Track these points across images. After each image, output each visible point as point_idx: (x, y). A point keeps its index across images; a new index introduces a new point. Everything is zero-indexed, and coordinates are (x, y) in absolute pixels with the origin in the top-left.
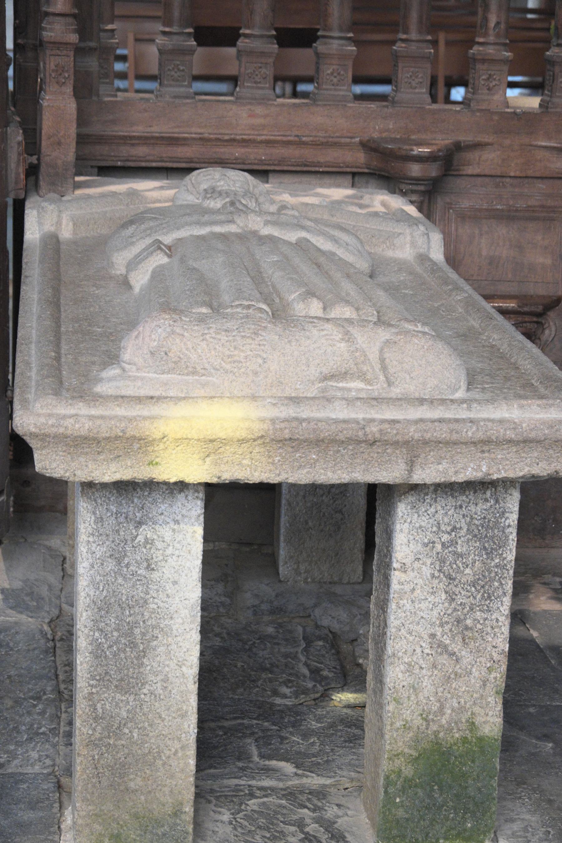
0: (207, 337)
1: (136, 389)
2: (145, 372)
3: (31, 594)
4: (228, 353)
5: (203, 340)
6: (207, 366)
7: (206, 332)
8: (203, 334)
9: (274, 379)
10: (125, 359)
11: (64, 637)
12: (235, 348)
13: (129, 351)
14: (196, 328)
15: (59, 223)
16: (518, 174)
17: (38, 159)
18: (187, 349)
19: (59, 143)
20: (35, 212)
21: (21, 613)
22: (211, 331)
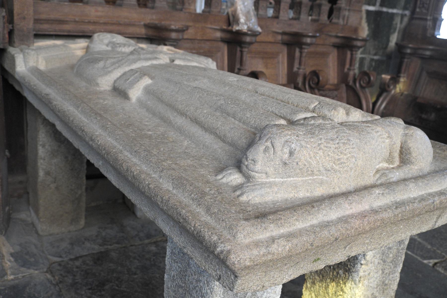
0: (322, 146)
1: (274, 194)
2: (272, 178)
3: (27, 253)
4: (337, 157)
5: (320, 149)
6: (322, 169)
7: (320, 142)
8: (319, 145)
9: (360, 171)
10: (256, 170)
11: (61, 280)
12: (341, 153)
13: (260, 163)
14: (312, 140)
15: (37, 61)
16: (201, 38)
17: (13, 27)
18: (311, 158)
19: (24, 18)
20: (21, 56)
21: (29, 268)
22: (323, 141)
